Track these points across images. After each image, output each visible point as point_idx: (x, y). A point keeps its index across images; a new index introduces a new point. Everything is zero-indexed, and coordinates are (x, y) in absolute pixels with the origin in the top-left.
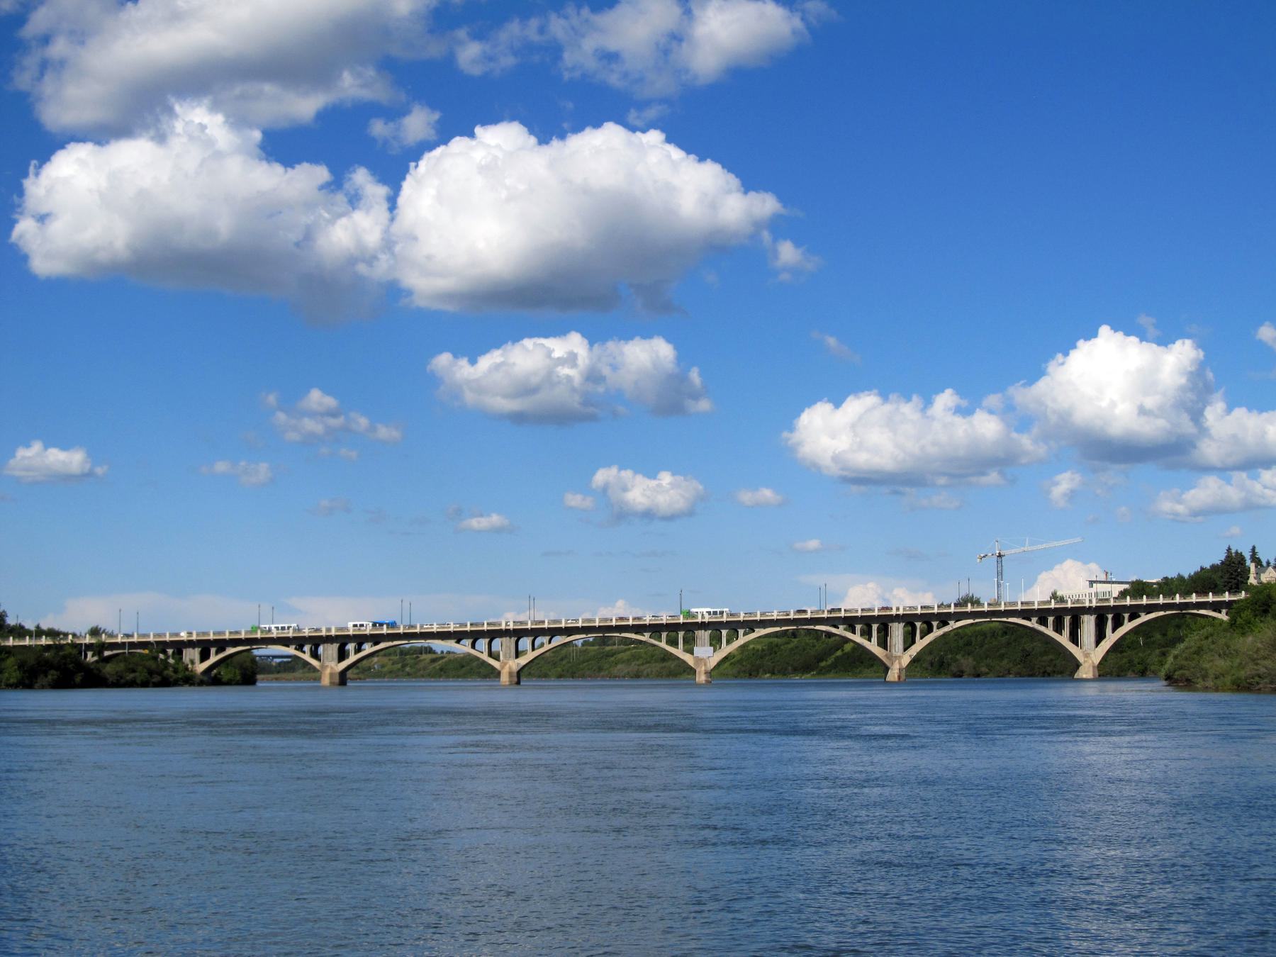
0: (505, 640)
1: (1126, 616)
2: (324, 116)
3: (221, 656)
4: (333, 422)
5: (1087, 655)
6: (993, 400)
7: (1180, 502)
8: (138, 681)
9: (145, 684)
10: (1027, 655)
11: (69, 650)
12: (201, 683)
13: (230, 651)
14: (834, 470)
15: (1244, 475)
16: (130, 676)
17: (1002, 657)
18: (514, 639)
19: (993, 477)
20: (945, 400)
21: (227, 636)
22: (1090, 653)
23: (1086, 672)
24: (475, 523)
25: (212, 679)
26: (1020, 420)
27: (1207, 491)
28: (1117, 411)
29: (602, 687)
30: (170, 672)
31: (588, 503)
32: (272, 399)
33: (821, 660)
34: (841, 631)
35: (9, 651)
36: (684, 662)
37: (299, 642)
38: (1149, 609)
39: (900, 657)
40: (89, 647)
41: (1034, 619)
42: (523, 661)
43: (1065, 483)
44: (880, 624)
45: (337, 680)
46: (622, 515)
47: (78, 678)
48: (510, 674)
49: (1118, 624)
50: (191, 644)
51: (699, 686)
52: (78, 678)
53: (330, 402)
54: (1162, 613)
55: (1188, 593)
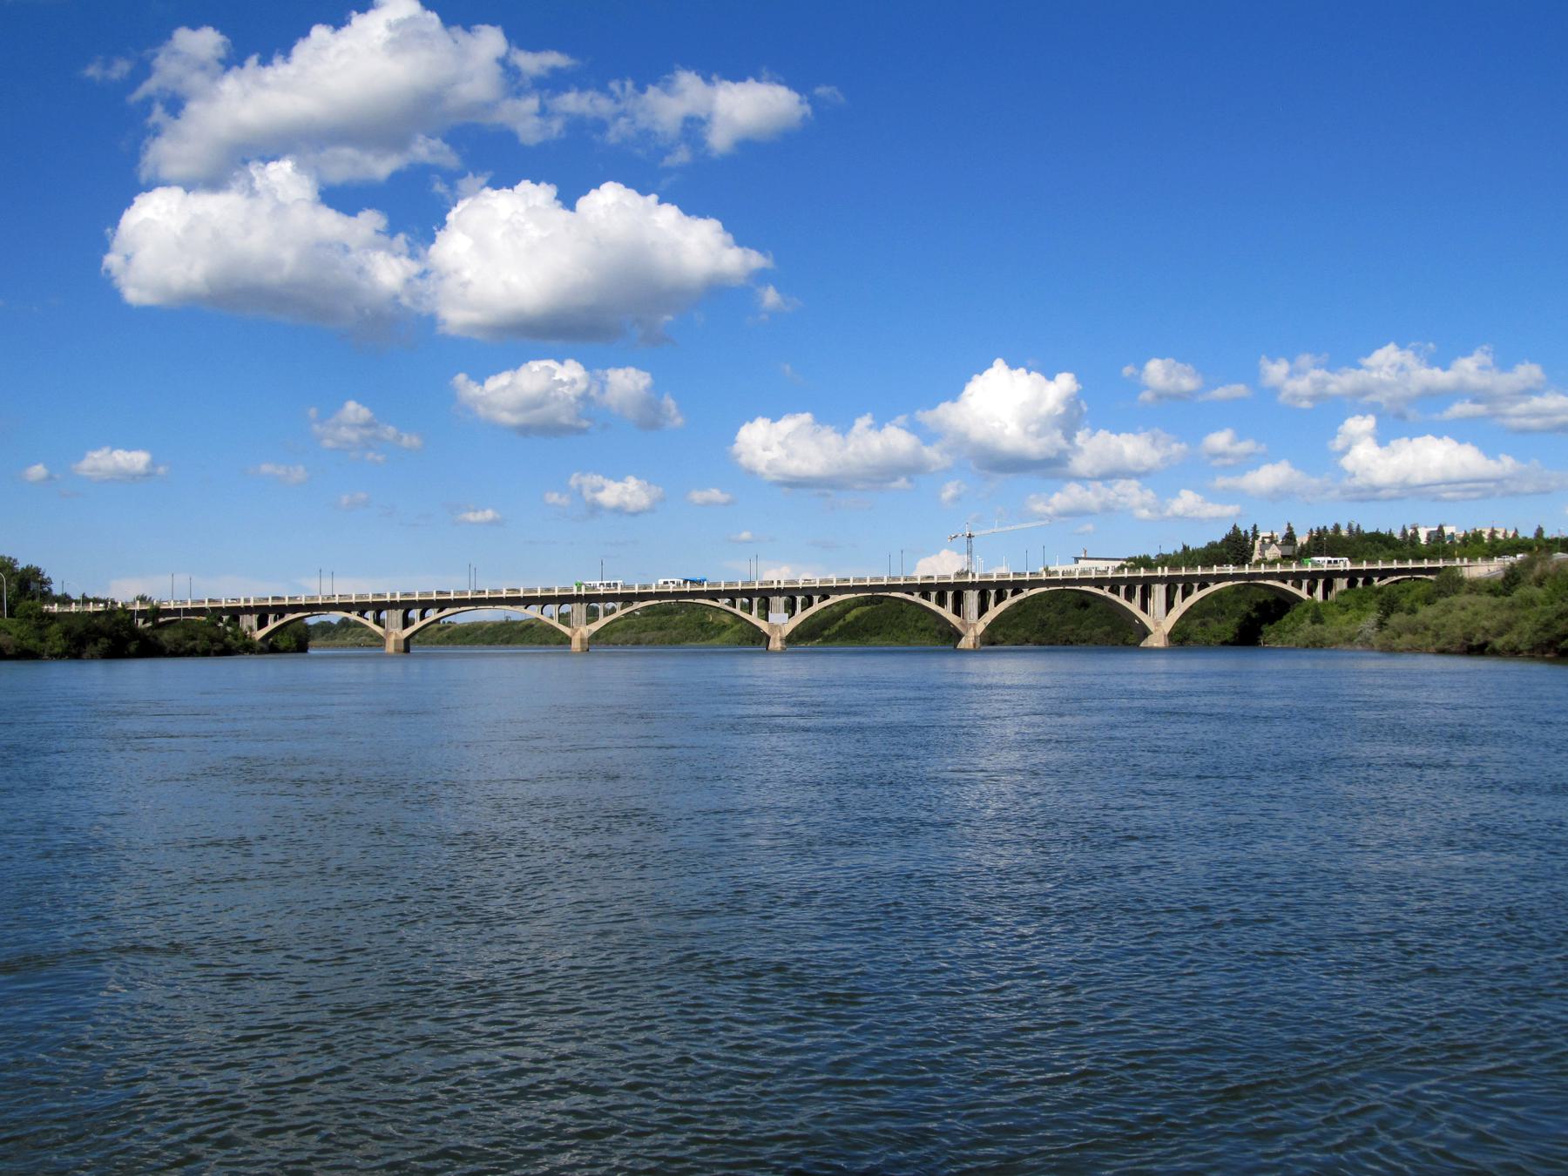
0: (576, 606)
1: (1009, 591)
2: (396, 177)
3: (280, 622)
4: (367, 432)
5: (1158, 624)
6: (901, 419)
7: (1048, 505)
8: (199, 649)
9: (206, 653)
10: (1043, 624)
11: (121, 616)
12: (262, 651)
13: (289, 617)
14: (772, 476)
15: (1099, 484)
16: (191, 644)
17: (1016, 626)
18: (400, 612)
19: (902, 482)
20: (863, 423)
21: (286, 602)
22: (1160, 620)
23: (1157, 640)
24: (471, 517)
25: (271, 647)
26: (928, 436)
27: (1069, 496)
28: (1007, 432)
29: (658, 654)
30: (230, 638)
31: (565, 501)
32: (313, 412)
33: (824, 629)
34: (1104, 592)
35: (53, 617)
36: (758, 629)
37: (362, 608)
38: (1219, 578)
39: (974, 625)
40: (142, 613)
41: (1107, 588)
42: (595, 627)
43: (949, 491)
44: (954, 591)
45: (402, 647)
46: (595, 509)
47: (132, 647)
48: (582, 640)
49: (1000, 598)
50: (248, 610)
51: (775, 653)
52: (132, 647)
53: (364, 413)
54: (1044, 589)
55: (1194, 566)
